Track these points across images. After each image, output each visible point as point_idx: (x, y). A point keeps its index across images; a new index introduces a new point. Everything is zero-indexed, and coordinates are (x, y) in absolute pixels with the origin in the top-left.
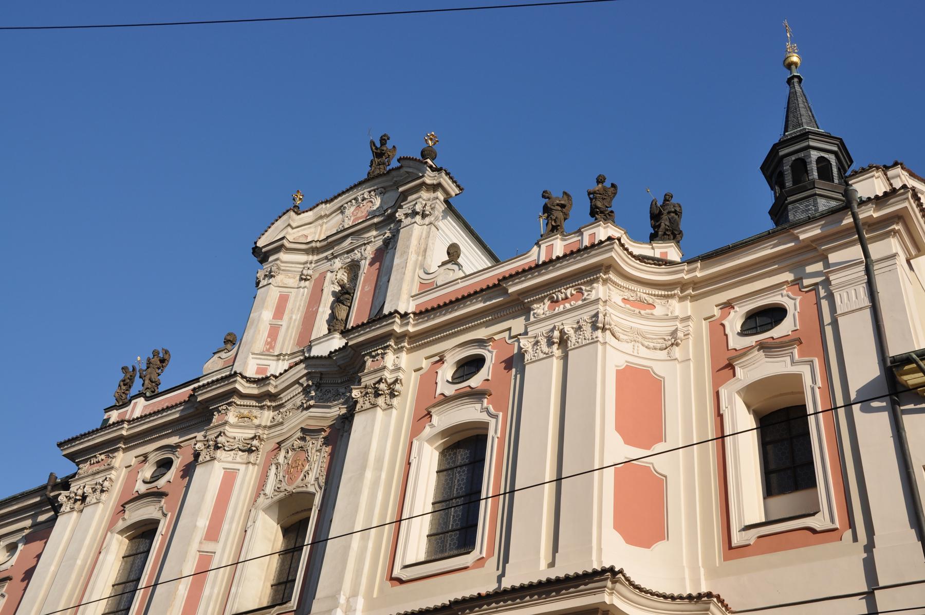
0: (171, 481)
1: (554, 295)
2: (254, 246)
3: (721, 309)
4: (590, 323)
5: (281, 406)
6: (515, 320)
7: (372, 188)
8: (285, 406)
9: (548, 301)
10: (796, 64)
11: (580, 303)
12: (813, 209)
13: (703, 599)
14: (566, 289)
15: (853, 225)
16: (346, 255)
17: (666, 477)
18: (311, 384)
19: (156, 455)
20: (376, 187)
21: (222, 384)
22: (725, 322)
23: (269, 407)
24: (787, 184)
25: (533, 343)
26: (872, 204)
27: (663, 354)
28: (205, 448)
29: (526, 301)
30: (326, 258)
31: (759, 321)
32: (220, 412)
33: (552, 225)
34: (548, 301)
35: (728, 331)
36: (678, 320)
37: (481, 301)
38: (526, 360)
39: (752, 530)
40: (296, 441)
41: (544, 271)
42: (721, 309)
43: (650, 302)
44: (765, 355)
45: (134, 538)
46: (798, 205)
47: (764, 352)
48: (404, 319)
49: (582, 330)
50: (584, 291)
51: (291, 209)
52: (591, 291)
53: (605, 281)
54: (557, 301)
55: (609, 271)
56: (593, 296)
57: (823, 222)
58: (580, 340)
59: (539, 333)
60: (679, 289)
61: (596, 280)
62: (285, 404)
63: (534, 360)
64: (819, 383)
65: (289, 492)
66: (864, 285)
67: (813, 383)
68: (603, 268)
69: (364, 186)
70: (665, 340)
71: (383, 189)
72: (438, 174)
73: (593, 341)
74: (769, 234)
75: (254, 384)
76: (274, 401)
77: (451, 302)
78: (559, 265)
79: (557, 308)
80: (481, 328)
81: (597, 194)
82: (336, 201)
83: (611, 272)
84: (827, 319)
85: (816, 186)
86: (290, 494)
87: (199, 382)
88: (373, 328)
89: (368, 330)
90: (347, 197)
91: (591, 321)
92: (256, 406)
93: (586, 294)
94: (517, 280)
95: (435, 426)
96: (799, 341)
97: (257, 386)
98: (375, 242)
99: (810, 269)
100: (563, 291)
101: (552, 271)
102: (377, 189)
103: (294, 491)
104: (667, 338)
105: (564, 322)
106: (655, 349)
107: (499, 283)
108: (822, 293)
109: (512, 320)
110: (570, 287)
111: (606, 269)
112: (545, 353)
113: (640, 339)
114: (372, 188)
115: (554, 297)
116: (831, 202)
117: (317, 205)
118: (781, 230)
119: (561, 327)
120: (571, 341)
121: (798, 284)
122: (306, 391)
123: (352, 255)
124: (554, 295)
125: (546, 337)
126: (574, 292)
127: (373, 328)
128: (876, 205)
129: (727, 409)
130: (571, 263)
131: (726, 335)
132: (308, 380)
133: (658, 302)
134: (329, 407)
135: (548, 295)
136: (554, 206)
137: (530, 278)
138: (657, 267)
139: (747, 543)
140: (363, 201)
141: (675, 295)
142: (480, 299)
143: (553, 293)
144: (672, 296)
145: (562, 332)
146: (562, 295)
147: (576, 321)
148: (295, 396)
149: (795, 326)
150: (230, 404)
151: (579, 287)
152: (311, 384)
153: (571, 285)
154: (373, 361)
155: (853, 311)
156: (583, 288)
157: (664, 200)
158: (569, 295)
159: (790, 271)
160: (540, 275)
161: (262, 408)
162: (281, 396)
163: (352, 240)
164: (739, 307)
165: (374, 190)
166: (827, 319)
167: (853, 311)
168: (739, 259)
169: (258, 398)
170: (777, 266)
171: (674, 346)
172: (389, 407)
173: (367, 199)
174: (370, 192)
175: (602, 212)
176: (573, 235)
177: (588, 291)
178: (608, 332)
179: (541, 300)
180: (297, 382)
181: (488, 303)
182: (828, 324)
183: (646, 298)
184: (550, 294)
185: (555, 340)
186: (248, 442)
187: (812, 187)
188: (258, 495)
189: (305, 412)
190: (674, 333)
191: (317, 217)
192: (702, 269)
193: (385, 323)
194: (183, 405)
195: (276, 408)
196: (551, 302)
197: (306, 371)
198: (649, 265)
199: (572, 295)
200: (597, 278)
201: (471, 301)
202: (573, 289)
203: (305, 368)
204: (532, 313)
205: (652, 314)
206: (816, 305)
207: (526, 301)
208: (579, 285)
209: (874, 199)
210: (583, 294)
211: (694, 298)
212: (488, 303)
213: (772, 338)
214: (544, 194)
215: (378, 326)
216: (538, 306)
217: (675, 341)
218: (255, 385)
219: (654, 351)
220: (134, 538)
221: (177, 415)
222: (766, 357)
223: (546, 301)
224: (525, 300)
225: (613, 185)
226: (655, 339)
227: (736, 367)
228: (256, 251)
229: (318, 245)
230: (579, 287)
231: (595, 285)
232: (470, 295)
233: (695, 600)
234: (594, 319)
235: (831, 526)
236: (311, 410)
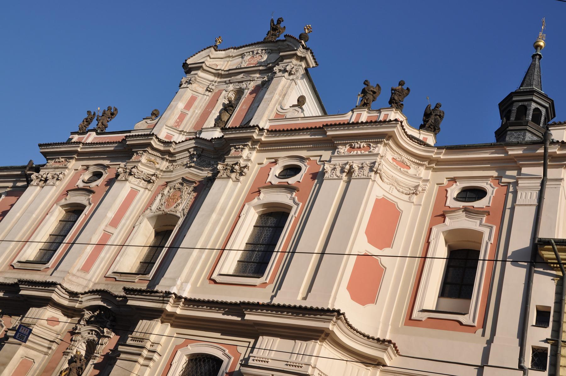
0: (99, 186)
1: (353, 144)
2: (185, 62)
3: (448, 181)
4: (369, 166)
5: (174, 161)
6: (326, 151)
7: (264, 48)
8: (177, 162)
9: (349, 146)
10: (541, 47)
11: (367, 153)
12: (522, 138)
13: (386, 343)
14: (362, 142)
15: (543, 154)
16: (237, 84)
17: (386, 268)
18: (195, 153)
19: (94, 168)
20: (267, 48)
21: (144, 138)
22: (449, 190)
23: (167, 160)
24: (511, 119)
25: (332, 168)
26: (558, 145)
27: (406, 197)
28: (123, 172)
29: (336, 142)
30: (225, 82)
31: (469, 194)
32: (138, 154)
33: (364, 102)
34: (349, 146)
35: (448, 195)
36: (421, 180)
37: (309, 134)
38: (325, 177)
39: (426, 313)
40: (177, 184)
41: (351, 128)
42: (448, 181)
43: (408, 165)
44: (466, 215)
45: (69, 212)
46: (514, 133)
47: (466, 213)
48: (261, 131)
49: (363, 169)
50: (371, 147)
51: (213, 46)
52: (376, 148)
53: (386, 145)
54: (354, 148)
55: (390, 139)
56: (376, 151)
57: (526, 148)
58: (360, 175)
59: (338, 164)
60: (428, 162)
61: (380, 142)
62: (177, 161)
63: (330, 178)
64: (492, 241)
65: (165, 212)
66: (538, 192)
67: (488, 240)
68: (387, 137)
69: (260, 46)
70: (410, 189)
71: (270, 51)
72: (306, 51)
73: (368, 177)
74: (491, 145)
75: (162, 144)
76: (171, 157)
77: (291, 130)
78: (361, 127)
79: (352, 152)
80: (305, 150)
81: (397, 91)
82: (240, 49)
83: (390, 140)
84: (509, 205)
85: (528, 125)
86: (166, 214)
87: (130, 133)
88: (241, 131)
89: (238, 132)
90: (244, 50)
91: (370, 165)
92: (160, 157)
93: (372, 148)
94: (334, 129)
95: (260, 200)
96: (488, 213)
97: (164, 145)
98: (257, 81)
99: (508, 173)
100: (359, 143)
101: (356, 129)
102: (267, 50)
103: (168, 212)
104: (411, 188)
105: (354, 161)
106: (403, 193)
107: (323, 127)
108: (511, 189)
109: (324, 151)
110: (364, 142)
111: (388, 137)
112: (337, 176)
113: (396, 184)
114: (264, 48)
115: (352, 145)
116: (534, 137)
117: (229, 49)
118: (499, 145)
119: (351, 164)
120: (355, 174)
121: (499, 180)
122: (191, 157)
123: (241, 85)
124: (353, 144)
125: (341, 167)
126: (365, 146)
127: (241, 131)
128: (561, 146)
129: (433, 240)
130: (365, 128)
131: (447, 197)
132: (194, 151)
133: (413, 166)
134: (202, 170)
135: (349, 143)
136: (369, 91)
137: (342, 130)
138: (419, 145)
139: (421, 319)
140: (257, 54)
141: (424, 164)
142: (309, 133)
143: (353, 142)
144: (422, 165)
145: (351, 167)
146: (358, 145)
147: (361, 163)
148: (184, 158)
149: (489, 204)
150: (145, 151)
151: (369, 143)
152: (195, 153)
153: (365, 141)
154: (235, 151)
155: (526, 205)
156: (372, 145)
157: (435, 107)
158: (362, 146)
159: (497, 171)
160: (348, 129)
161: (163, 159)
162: (176, 155)
163: (243, 76)
164: (460, 183)
165: (265, 50)
166: (509, 205)
167: (526, 205)
168: (468, 155)
169: (163, 153)
170: (490, 165)
171: (414, 194)
172: (237, 180)
173: (260, 54)
174: (262, 50)
175: (396, 103)
176: (375, 112)
177: (374, 147)
178: (378, 175)
179: (345, 144)
180: (187, 150)
181: (313, 137)
182: (509, 209)
183: (407, 162)
184: (351, 142)
185: (346, 170)
186: (149, 176)
187: (526, 125)
188: (147, 209)
189: (187, 169)
190: (416, 187)
191: (227, 56)
192: (445, 154)
193: (249, 131)
194: (117, 144)
195: (171, 162)
196: (350, 147)
197: (195, 145)
198: (414, 143)
199: (364, 147)
200: (382, 141)
201: (303, 133)
202: (365, 143)
203: (195, 143)
204: (337, 150)
205: (407, 172)
206: (505, 195)
207: (336, 142)
208: (369, 142)
209: (560, 142)
210: (370, 148)
211: (435, 170)
212: (313, 137)
213: (473, 207)
214: (365, 82)
215: (244, 131)
216: (342, 147)
217: (415, 192)
218: (162, 145)
219: (402, 194)
220: (69, 212)
221: (112, 149)
222: (466, 217)
223: (347, 146)
224: (335, 141)
225: (408, 89)
226: (404, 187)
227: (446, 217)
228: (185, 65)
229: (223, 73)
230: (369, 143)
231: (379, 145)
232: (303, 129)
233: (381, 342)
234: (372, 165)
235: (472, 324)
236: (191, 169)
